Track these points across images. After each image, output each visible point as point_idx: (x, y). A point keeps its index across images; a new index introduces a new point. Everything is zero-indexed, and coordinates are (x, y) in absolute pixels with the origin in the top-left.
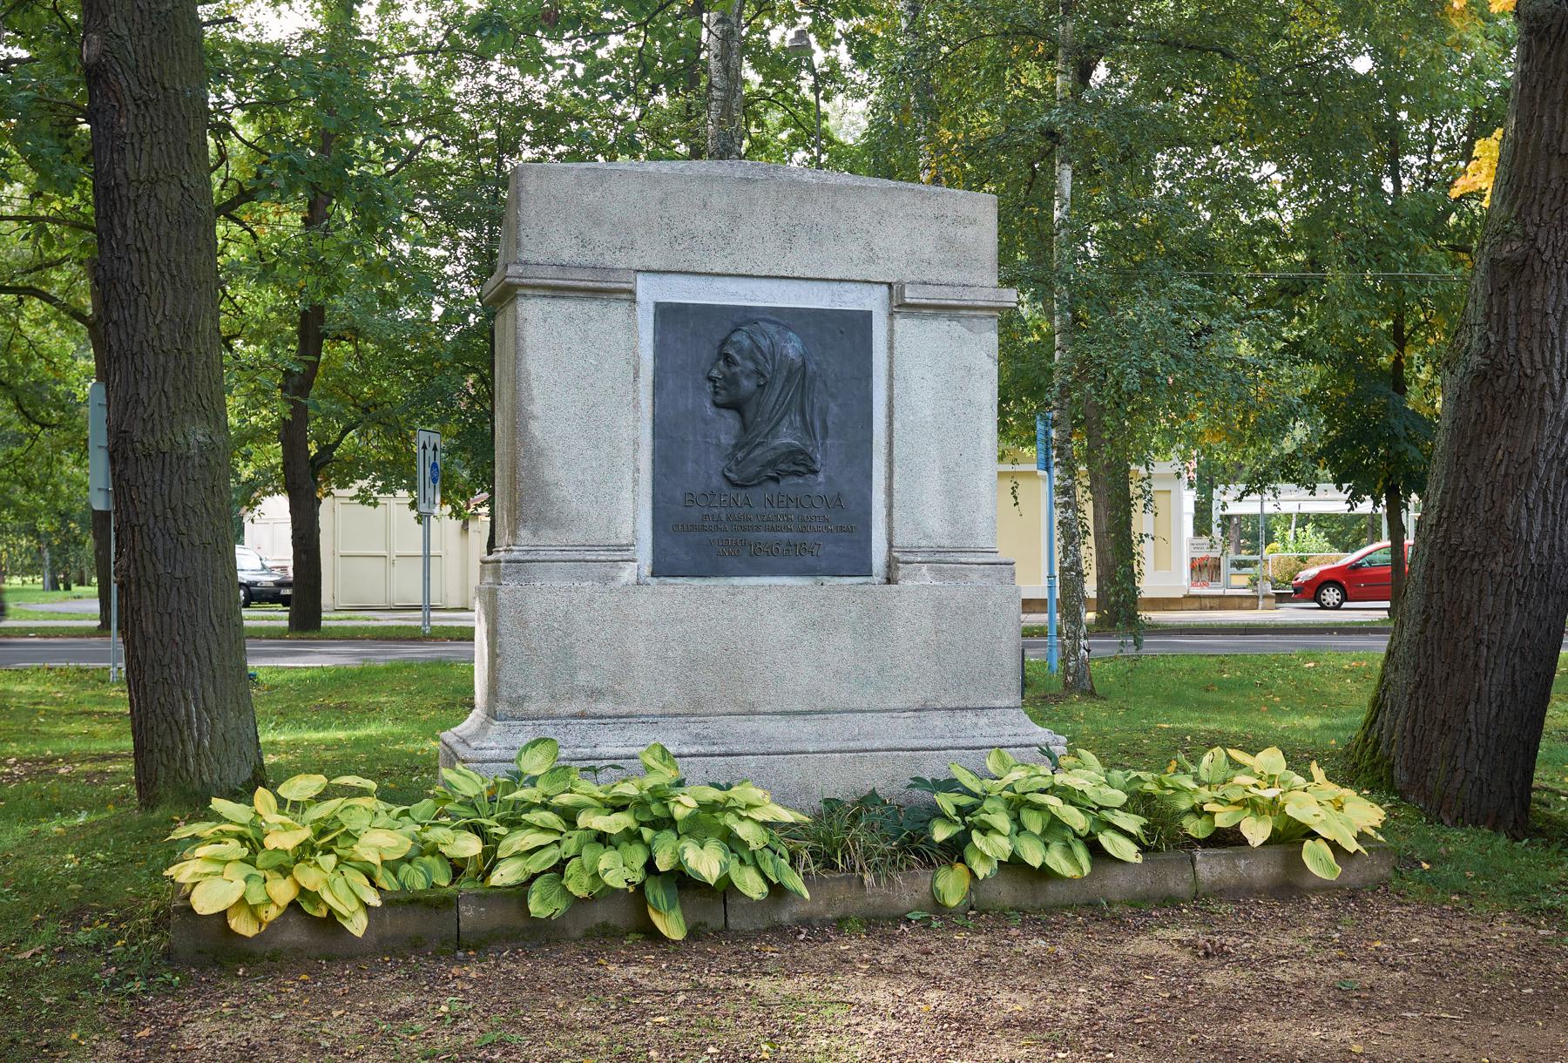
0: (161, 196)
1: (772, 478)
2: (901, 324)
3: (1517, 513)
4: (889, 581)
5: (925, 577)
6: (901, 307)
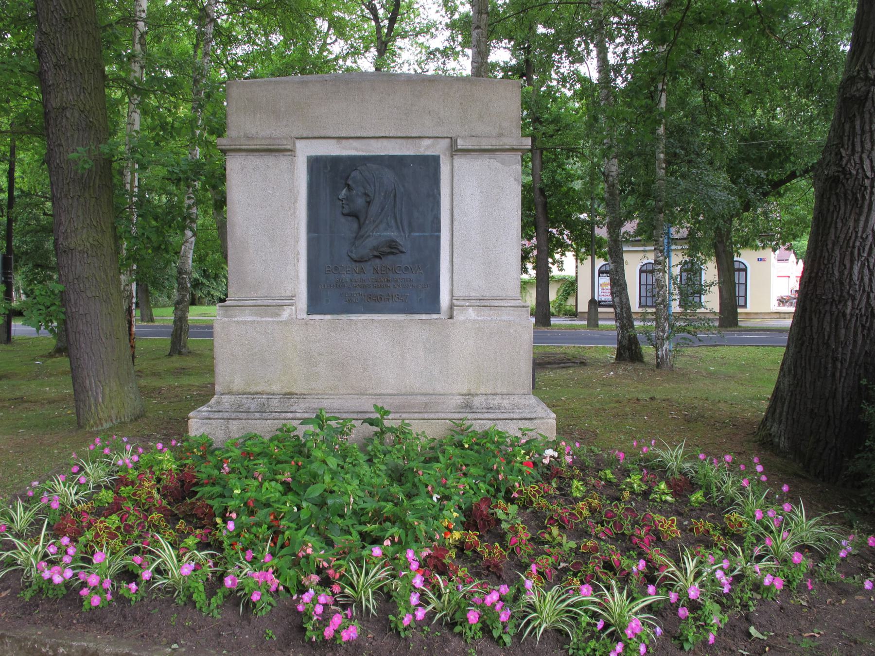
0: (68, 115)
1: (376, 257)
2: (459, 161)
3: (861, 272)
4: (451, 317)
5: (471, 313)
6: (455, 151)
